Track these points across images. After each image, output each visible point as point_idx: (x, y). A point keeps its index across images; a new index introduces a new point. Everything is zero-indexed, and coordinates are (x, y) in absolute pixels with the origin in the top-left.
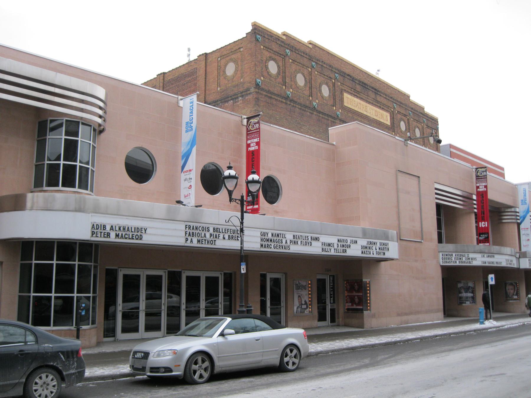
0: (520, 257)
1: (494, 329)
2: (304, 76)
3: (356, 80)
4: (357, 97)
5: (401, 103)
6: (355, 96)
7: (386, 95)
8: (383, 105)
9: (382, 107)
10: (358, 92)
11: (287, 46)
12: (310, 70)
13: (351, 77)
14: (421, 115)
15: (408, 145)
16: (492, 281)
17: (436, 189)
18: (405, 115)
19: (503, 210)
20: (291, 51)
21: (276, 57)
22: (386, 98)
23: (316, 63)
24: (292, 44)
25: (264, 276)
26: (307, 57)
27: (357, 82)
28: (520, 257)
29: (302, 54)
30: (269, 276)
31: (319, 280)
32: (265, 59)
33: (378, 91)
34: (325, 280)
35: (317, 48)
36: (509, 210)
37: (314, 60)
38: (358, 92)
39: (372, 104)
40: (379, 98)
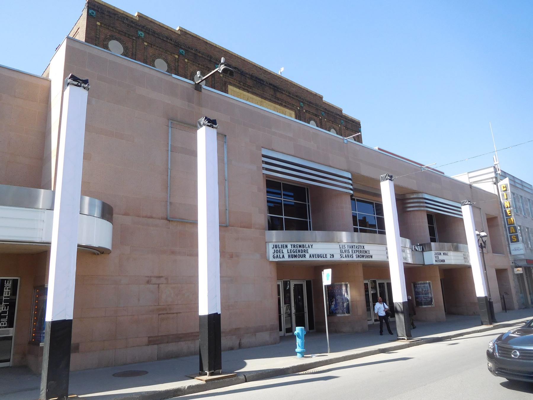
0: (423, 251)
1: (302, 373)
2: (167, 62)
3: (247, 74)
4: (248, 92)
5: (310, 103)
6: (244, 90)
7: (290, 93)
8: (289, 104)
9: (284, 104)
10: (249, 86)
11: (140, 28)
12: (177, 56)
13: (239, 70)
14: (338, 117)
15: (202, 89)
16: (328, 279)
17: (264, 156)
18: (316, 115)
19: (408, 196)
20: (145, 32)
21: (122, 37)
22: (289, 96)
23: (186, 50)
24: (149, 27)
25: (375, 282)
26: (172, 43)
27: (248, 76)
28: (423, 251)
29: (165, 39)
30: (293, 284)
31: (365, 284)
32: (103, 37)
33: (278, 88)
34: (302, 285)
35: (188, 36)
36: (415, 196)
37: (182, 47)
38: (249, 86)
39: (270, 100)
40: (278, 95)
